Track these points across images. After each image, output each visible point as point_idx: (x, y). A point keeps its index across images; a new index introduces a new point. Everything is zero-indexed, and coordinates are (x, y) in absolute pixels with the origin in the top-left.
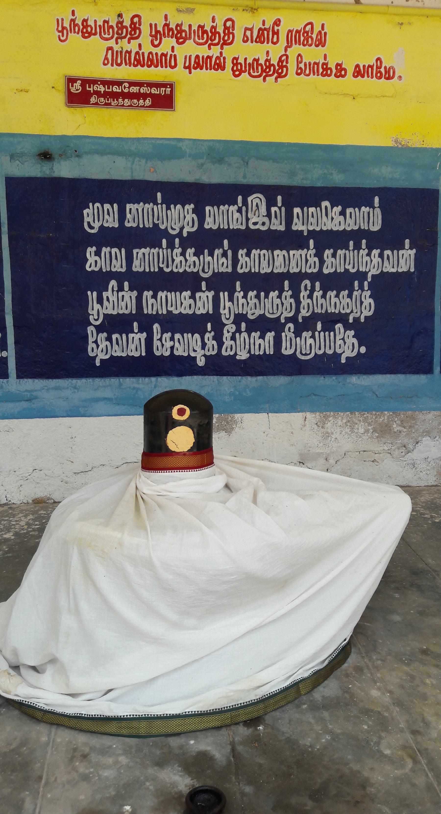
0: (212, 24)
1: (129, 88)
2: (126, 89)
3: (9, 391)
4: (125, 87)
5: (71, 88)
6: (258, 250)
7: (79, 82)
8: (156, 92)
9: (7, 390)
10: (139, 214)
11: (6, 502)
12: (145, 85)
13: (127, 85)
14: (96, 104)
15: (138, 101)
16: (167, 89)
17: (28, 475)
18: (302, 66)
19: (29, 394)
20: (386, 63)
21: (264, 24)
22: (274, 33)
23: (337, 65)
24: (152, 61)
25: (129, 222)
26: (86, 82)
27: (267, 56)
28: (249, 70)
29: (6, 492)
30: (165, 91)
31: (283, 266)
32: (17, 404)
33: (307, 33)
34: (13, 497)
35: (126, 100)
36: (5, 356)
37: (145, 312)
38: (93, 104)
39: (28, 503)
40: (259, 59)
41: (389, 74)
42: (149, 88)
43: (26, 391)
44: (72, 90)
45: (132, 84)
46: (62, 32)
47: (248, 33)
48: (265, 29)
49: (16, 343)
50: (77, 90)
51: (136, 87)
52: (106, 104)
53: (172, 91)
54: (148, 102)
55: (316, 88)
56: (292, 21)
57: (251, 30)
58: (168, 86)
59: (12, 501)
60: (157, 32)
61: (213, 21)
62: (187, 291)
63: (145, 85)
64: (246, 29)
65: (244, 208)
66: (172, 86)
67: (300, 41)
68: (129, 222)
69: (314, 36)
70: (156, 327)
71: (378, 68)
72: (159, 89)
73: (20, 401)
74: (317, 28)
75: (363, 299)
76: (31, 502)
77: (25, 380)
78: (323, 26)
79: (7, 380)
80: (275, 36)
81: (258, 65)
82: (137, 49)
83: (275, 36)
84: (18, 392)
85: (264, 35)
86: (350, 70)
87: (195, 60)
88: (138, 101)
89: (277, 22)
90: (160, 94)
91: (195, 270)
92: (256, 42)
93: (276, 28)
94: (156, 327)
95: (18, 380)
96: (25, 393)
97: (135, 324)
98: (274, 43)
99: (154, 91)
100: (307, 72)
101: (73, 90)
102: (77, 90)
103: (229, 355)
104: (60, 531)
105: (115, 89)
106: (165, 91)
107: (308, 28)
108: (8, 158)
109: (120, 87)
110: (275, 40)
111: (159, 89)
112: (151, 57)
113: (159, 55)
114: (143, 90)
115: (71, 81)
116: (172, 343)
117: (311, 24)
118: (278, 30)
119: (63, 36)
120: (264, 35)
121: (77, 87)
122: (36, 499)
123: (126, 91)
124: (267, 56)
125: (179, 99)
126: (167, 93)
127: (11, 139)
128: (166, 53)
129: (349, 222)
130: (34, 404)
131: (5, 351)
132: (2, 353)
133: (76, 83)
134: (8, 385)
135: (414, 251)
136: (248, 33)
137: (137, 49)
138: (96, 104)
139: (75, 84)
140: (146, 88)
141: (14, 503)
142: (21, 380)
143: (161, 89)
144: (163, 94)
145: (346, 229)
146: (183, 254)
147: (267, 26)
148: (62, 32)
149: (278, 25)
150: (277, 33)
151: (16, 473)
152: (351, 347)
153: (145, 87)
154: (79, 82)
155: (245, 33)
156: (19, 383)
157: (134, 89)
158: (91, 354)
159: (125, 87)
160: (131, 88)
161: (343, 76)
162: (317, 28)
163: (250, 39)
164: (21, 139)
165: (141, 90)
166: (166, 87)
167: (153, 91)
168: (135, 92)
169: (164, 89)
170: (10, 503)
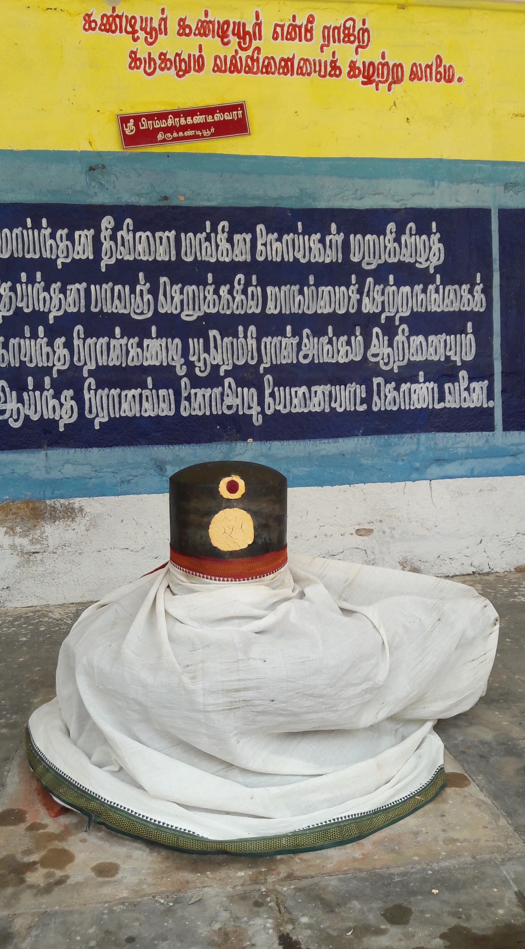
0: (161, 16)
3: (495, 445)
5: (125, 129)
7: (132, 121)
9: (493, 444)
11: (489, 570)
12: (218, 111)
14: (164, 140)
15: (172, 134)
16: (239, 112)
17: (511, 539)
18: (441, 69)
19: (515, 448)
20: (446, 62)
21: (206, 14)
22: (307, 31)
23: (162, 54)
24: (235, 66)
25: (78, 253)
27: (334, 57)
28: (145, 67)
29: (488, 559)
31: (328, 306)
32: (503, 459)
33: (349, 29)
34: (495, 565)
36: (491, 406)
39: (510, 572)
41: (447, 76)
42: (222, 114)
43: (513, 445)
45: (177, 114)
46: (150, 34)
47: (279, 29)
48: (117, 16)
49: (503, 391)
56: (329, 17)
57: (282, 27)
58: (239, 109)
59: (495, 569)
60: (246, 33)
64: (276, 25)
65: (213, 235)
68: (78, 253)
71: (438, 66)
73: (506, 456)
75: (340, 348)
76: (513, 570)
77: (512, 432)
79: (493, 433)
81: (181, 61)
82: (331, 58)
84: (504, 446)
85: (295, 32)
86: (345, 69)
87: (231, 61)
88: (172, 134)
89: (311, 19)
90: (233, 119)
92: (287, 39)
93: (310, 25)
95: (504, 433)
96: (512, 447)
97: (421, 373)
98: (307, 40)
100: (255, 70)
101: (128, 132)
102: (132, 131)
103: (303, 412)
106: (179, 121)
108: (502, 188)
112: (234, 62)
115: (124, 120)
118: (312, 28)
119: (245, 44)
120: (295, 32)
122: (518, 567)
127: (506, 168)
128: (291, 57)
129: (405, 252)
130: (518, 459)
131: (492, 401)
132: (489, 402)
133: (129, 122)
134: (494, 439)
137: (331, 58)
138: (164, 140)
139: (128, 124)
141: (497, 572)
142: (508, 433)
143: (234, 113)
146: (216, 292)
147: (298, 22)
148: (150, 34)
150: (311, 31)
151: (500, 537)
152: (69, 412)
153: (218, 113)
154: (132, 121)
155: (275, 29)
156: (506, 436)
161: (338, 76)
163: (119, 28)
164: (515, 168)
170: (493, 571)
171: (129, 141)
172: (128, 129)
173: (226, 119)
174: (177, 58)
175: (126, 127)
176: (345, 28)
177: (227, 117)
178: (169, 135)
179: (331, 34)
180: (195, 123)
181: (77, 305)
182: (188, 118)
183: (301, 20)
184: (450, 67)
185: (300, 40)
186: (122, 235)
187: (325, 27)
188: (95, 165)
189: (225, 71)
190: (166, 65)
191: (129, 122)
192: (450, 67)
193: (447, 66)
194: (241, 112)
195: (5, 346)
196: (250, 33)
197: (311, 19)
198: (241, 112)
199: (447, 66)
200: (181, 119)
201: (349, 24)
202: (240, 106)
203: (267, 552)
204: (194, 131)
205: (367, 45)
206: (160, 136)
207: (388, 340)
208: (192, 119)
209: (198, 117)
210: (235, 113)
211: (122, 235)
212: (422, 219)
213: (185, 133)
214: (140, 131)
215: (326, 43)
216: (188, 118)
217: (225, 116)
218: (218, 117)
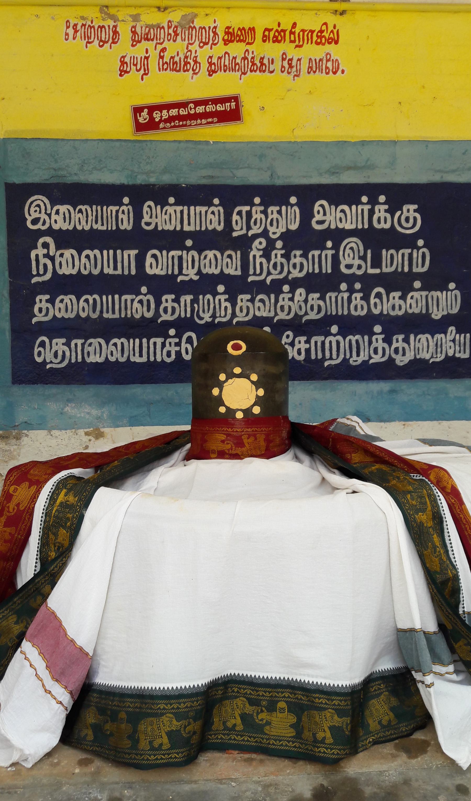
1: (195, 108)
2: (192, 110)
4: (191, 109)
5: (139, 118)
7: (146, 110)
13: (192, 105)
14: (164, 128)
15: (170, 124)
16: (232, 104)
26: (152, 109)
30: (230, 105)
35: (203, 120)
38: (162, 129)
42: (214, 105)
44: (140, 121)
45: (198, 103)
50: (145, 119)
51: (202, 107)
53: (237, 105)
55: (288, 91)
58: (233, 101)
61: (147, 52)
66: (236, 99)
72: (224, 104)
74: (330, 28)
88: (170, 124)
90: (225, 110)
99: (220, 108)
101: (141, 120)
102: (145, 119)
105: (183, 112)
106: (230, 105)
109: (186, 109)
111: (224, 104)
113: (318, 61)
114: (210, 108)
115: (137, 110)
116: (307, 346)
117: (325, 24)
121: (144, 117)
123: (192, 112)
125: (245, 111)
126: (232, 108)
133: (143, 112)
138: (164, 128)
139: (142, 114)
140: (211, 106)
143: (226, 104)
144: (228, 110)
145: (164, 228)
149: (163, 52)
153: (210, 105)
154: (146, 110)
157: (200, 109)
158: (39, 360)
160: (197, 109)
162: (330, 28)
165: (180, 111)
166: (231, 102)
167: (219, 109)
168: (174, 115)
169: (229, 104)
171: (139, 127)
172: (142, 118)
173: (219, 110)
174: (172, 60)
175: (140, 116)
178: (168, 124)
180: (198, 112)
181: (217, 301)
182: (163, 111)
184: (337, 60)
186: (44, 219)
188: (109, 146)
189: (179, 71)
190: (321, 40)
191: (143, 112)
192: (337, 60)
194: (234, 103)
198: (234, 103)
199: (334, 60)
200: (232, 104)
202: (236, 99)
205: (253, 43)
206: (161, 125)
208: (168, 112)
210: (228, 104)
211: (44, 219)
214: (148, 118)
216: (163, 111)
217: (218, 107)
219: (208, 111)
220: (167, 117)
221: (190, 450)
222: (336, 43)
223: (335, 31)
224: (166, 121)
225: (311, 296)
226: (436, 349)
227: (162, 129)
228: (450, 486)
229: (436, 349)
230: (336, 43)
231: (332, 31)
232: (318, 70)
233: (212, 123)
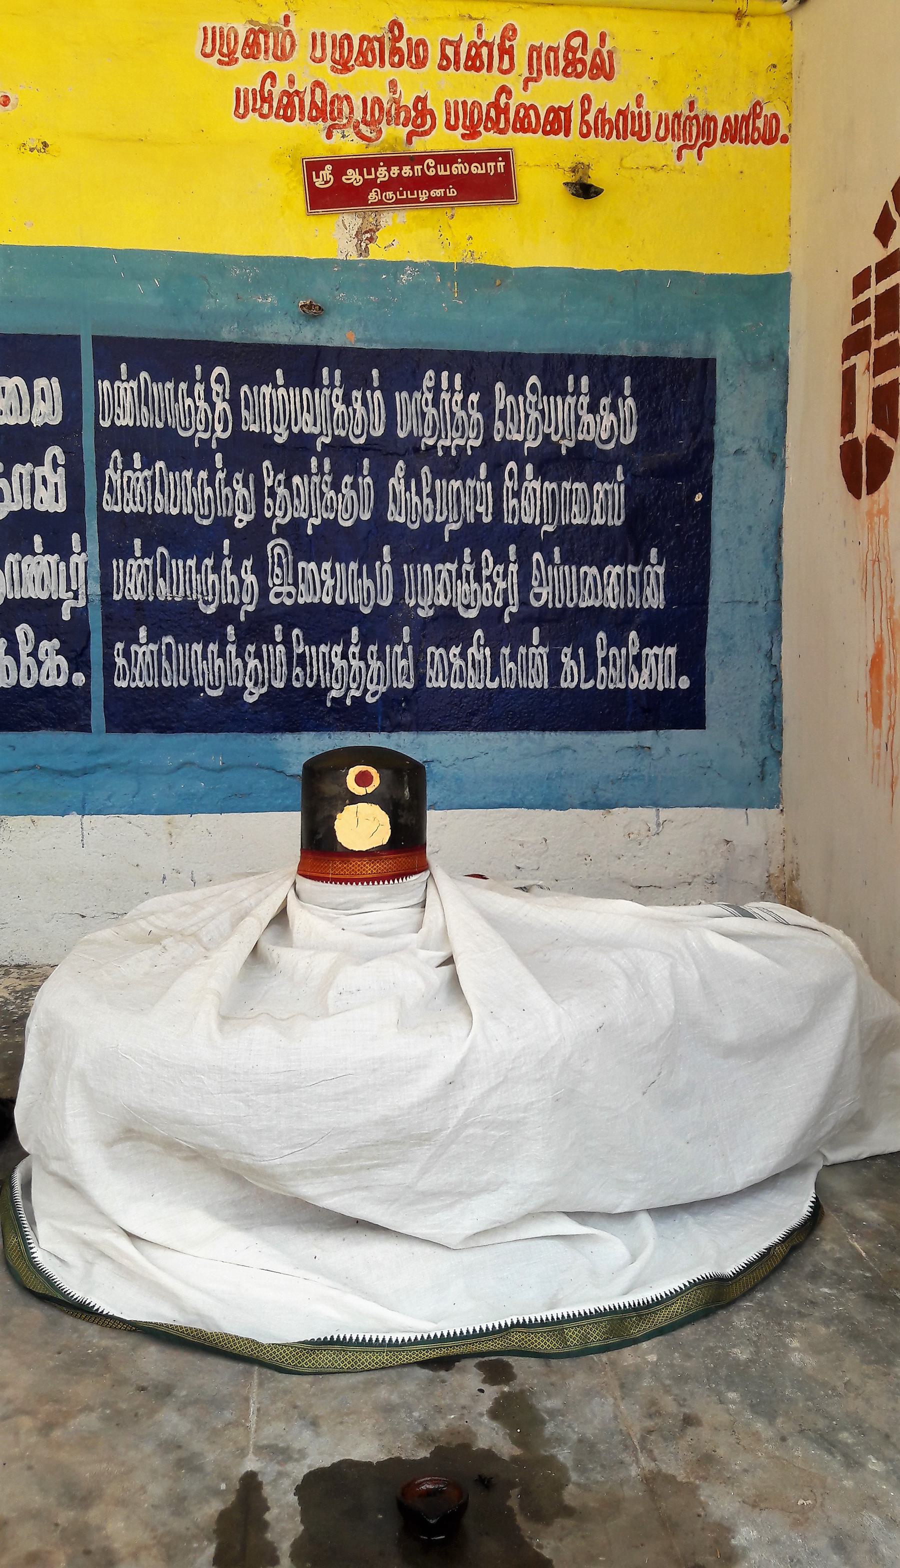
4: (429, 167)
5: (315, 180)
6: (29, 465)
7: (329, 167)
8: (480, 172)
10: (279, 408)
12: (459, 160)
13: (431, 162)
14: (381, 202)
16: (499, 164)
22: (503, 51)
30: (496, 167)
33: (574, 51)
37: (506, 521)
38: (372, 204)
40: (426, 98)
42: (466, 164)
47: (450, 51)
48: (485, 43)
50: (327, 182)
52: (398, 202)
53: (508, 167)
54: (374, 196)
56: (543, 29)
57: (457, 45)
58: (500, 159)
62: (53, 555)
63: (459, 160)
67: (557, 67)
69: (588, 59)
70: (23, 631)
78: (603, 37)
80: (506, 58)
83: (506, 58)
89: (510, 32)
91: (589, 438)
93: (508, 44)
94: (23, 631)
101: (319, 183)
102: (327, 182)
104: (55, 974)
106: (496, 167)
107: (576, 42)
110: (506, 65)
115: (313, 167)
118: (512, 46)
123: (431, 173)
124: (395, 93)
135: (547, 649)
136: (450, 51)
138: (381, 202)
139: (321, 173)
140: (461, 165)
143: (489, 164)
147: (487, 36)
150: (510, 52)
154: (329, 167)
155: (443, 50)
159: (429, 167)
162: (593, 44)
169: (493, 164)
175: (318, 177)
176: (569, 48)
177: (476, 169)
179: (542, 61)
182: (404, 168)
183: (493, 34)
185: (457, 69)
187: (532, 48)
193: (562, 134)
194: (503, 164)
195: (7, 474)
196: (403, 52)
197: (510, 32)
198: (503, 164)
199: (562, 134)
200: (499, 164)
201: (576, 42)
203: (406, 850)
204: (443, 190)
206: (373, 196)
207: (471, 554)
209: (459, 166)
212: (605, 374)
213: (432, 192)
215: (535, 75)
216: (404, 168)
217: (473, 168)
218: (458, 168)
219: (455, 173)
220: (387, 178)
221: (361, 635)
222: (609, 77)
223: (604, 51)
224: (384, 187)
225: (45, 645)
226: (226, 714)
227: (372, 204)
228: (326, 814)
229: (226, 714)
230: (609, 77)
231: (598, 53)
232: (671, 118)
233: (444, 199)
